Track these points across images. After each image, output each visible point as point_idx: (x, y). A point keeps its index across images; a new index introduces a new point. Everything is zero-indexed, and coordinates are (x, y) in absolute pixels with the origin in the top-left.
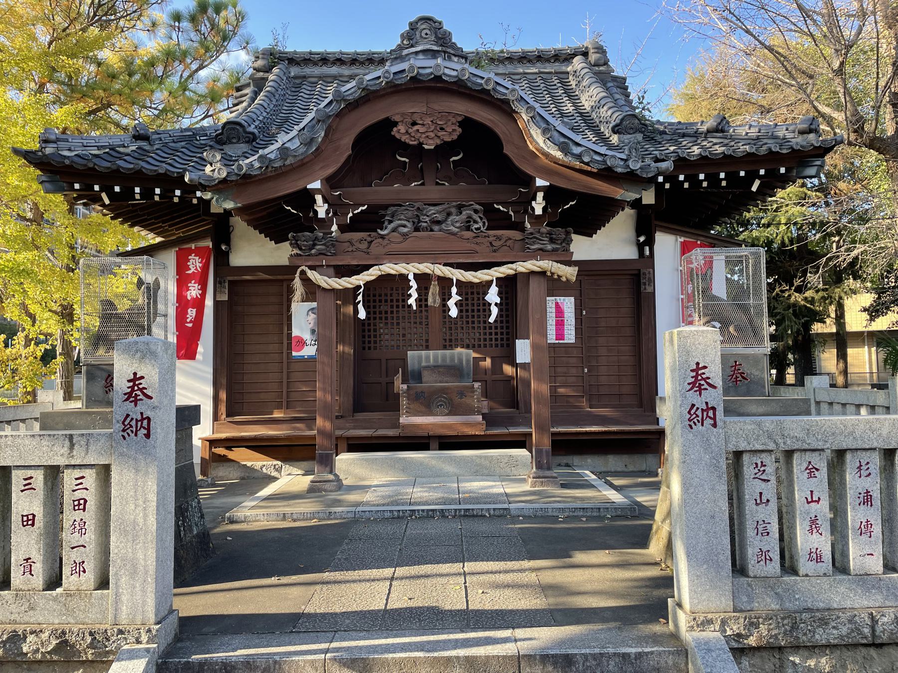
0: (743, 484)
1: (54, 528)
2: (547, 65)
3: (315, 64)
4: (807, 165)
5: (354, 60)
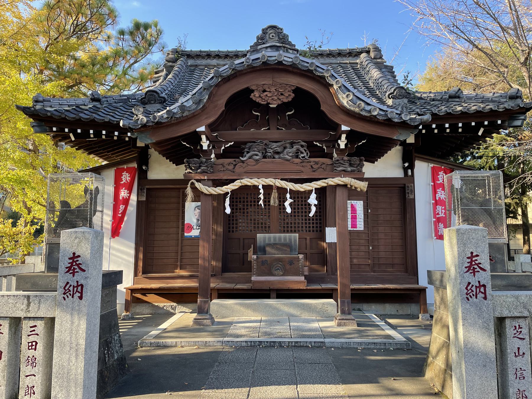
0: (506, 341)
1: (16, 361)
2: (344, 58)
3: (203, 58)
4: (516, 119)
5: (227, 56)
